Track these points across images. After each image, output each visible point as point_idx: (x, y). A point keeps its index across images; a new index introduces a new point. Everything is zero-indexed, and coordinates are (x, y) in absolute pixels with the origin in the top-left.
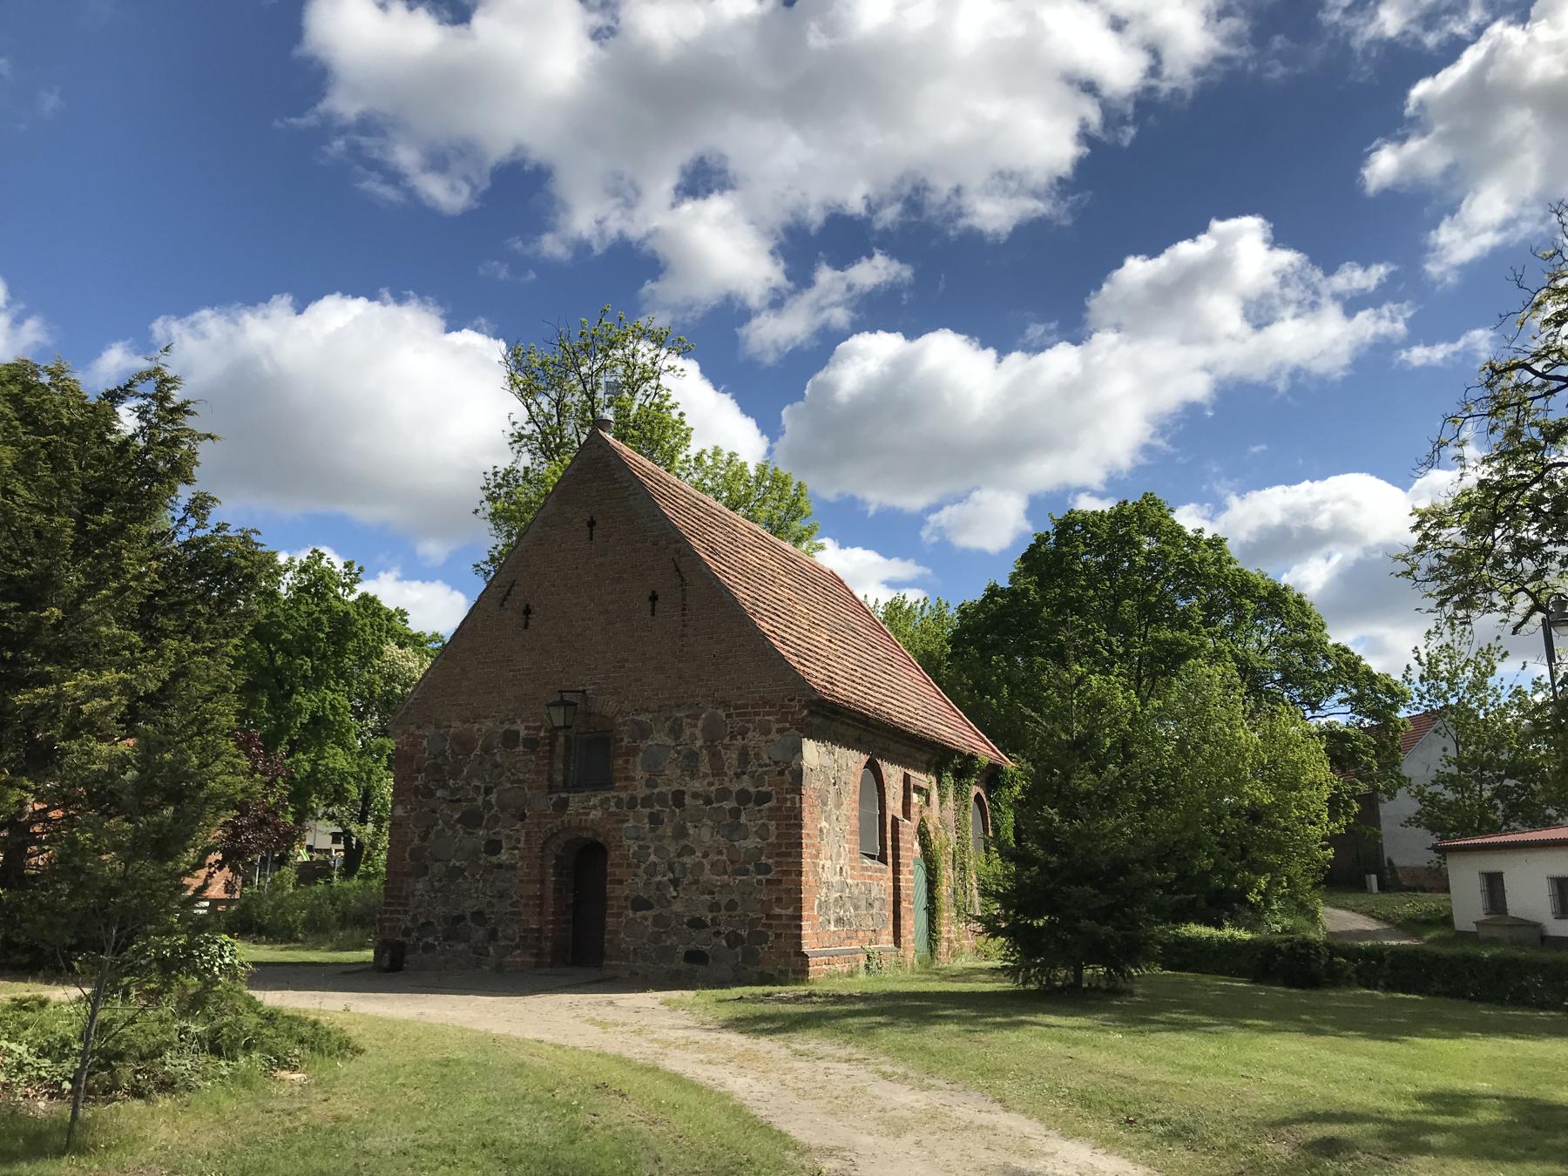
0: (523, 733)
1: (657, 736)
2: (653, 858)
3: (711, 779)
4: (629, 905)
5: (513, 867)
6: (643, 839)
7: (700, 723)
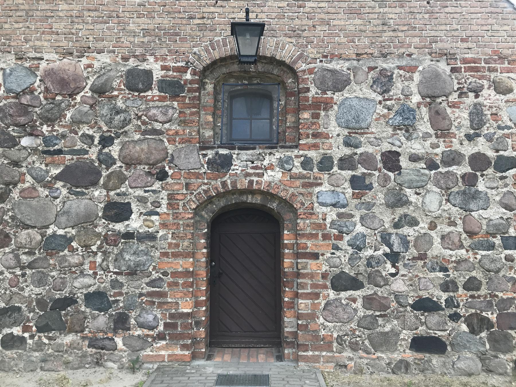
0: (158, 74)
1: (357, 88)
2: (359, 229)
3: (434, 140)
4: (329, 284)
5: (151, 237)
6: (344, 206)
7: (417, 77)
